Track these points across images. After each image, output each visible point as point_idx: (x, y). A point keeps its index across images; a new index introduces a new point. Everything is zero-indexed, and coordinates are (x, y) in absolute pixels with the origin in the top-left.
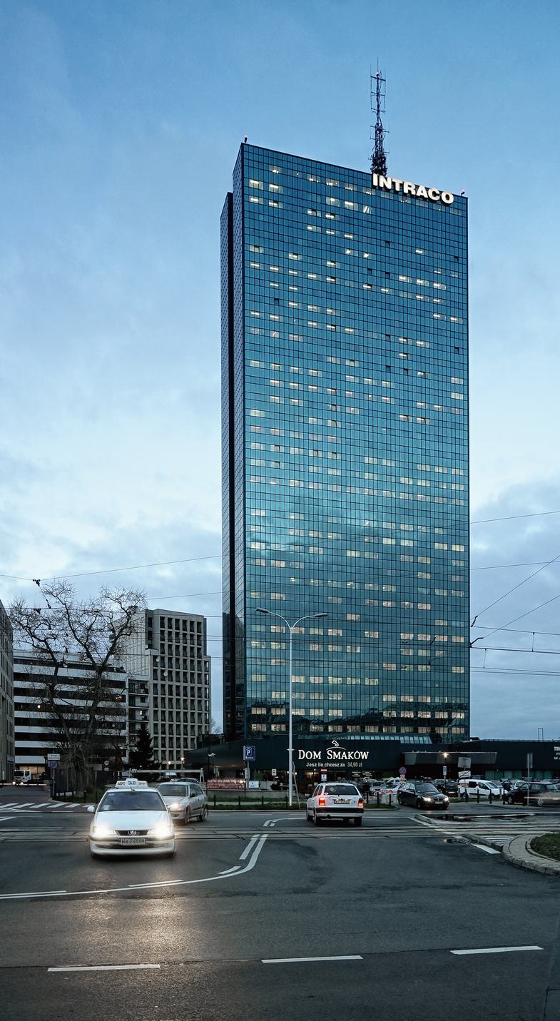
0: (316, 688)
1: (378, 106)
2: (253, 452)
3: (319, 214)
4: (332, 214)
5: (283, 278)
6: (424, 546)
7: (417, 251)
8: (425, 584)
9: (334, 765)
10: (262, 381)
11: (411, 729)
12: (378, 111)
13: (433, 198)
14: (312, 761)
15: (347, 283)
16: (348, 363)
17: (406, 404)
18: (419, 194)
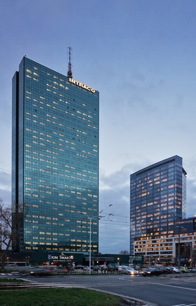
0: (48, 236)
1: (70, 57)
2: (27, 158)
3: (51, 86)
4: (55, 87)
5: (38, 104)
6: (84, 194)
7: (83, 105)
8: (85, 206)
9: (62, 261)
10: (30, 135)
11: (69, 250)
12: (70, 59)
13: (89, 90)
14: (55, 259)
15: (60, 110)
16: (60, 135)
17: (79, 151)
18: (84, 87)
